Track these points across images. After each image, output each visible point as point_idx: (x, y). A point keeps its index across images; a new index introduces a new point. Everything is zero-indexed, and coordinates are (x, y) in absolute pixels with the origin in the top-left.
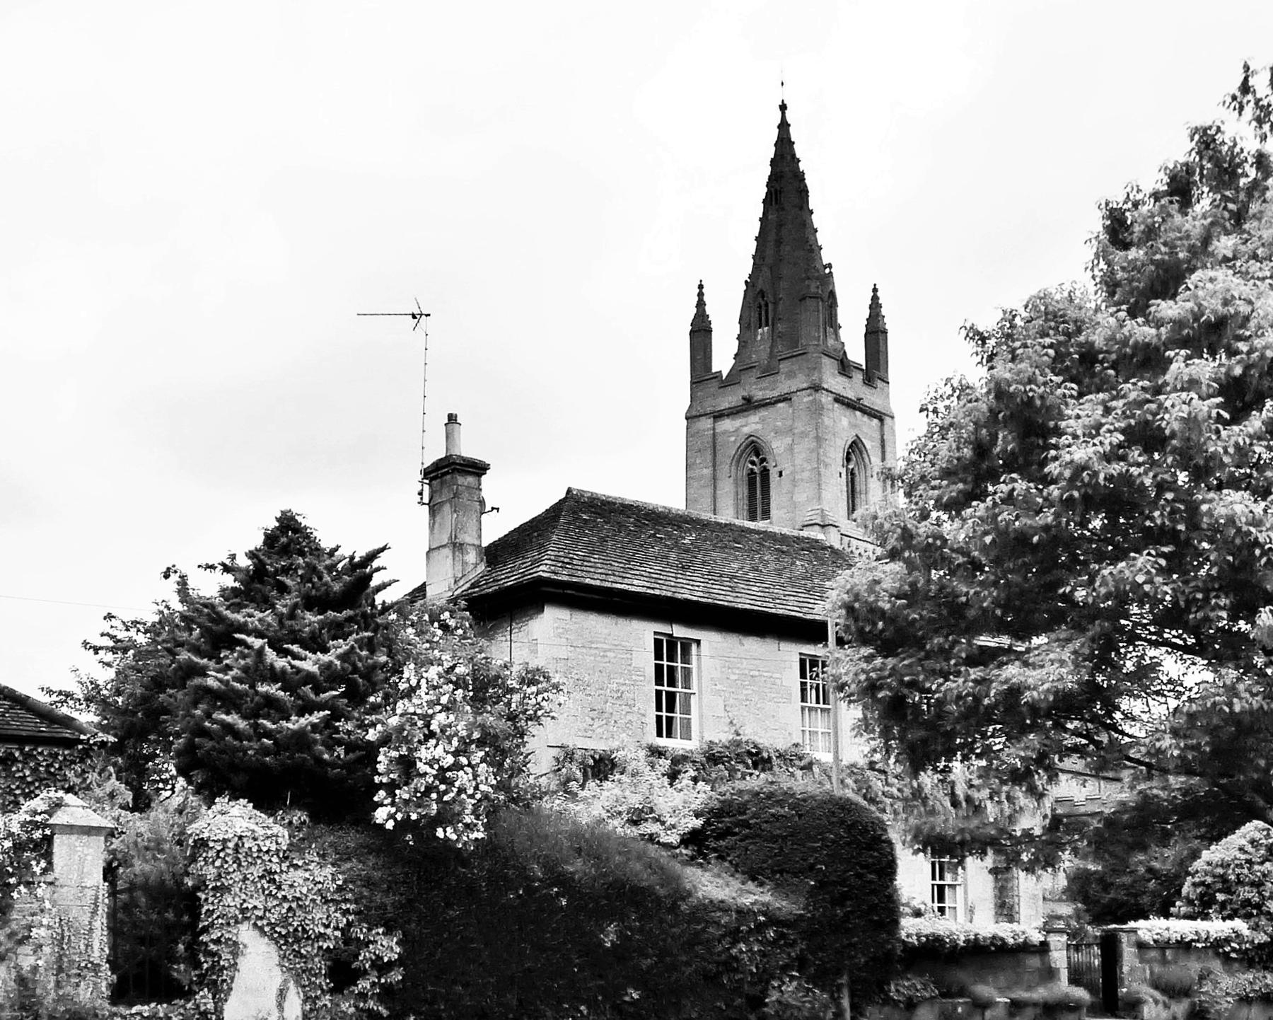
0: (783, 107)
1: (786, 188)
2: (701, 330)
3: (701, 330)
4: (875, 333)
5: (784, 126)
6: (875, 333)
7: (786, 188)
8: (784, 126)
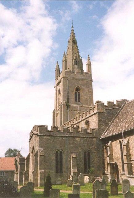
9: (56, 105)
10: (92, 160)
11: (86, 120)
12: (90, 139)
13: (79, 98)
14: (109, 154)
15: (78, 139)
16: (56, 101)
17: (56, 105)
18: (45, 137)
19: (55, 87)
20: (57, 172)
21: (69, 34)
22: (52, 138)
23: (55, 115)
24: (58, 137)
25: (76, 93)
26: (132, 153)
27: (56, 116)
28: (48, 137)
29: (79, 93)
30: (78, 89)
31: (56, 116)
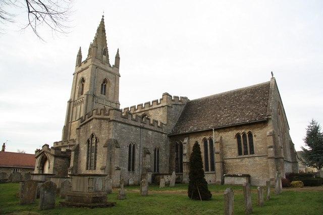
0: (103, 16)
1: (101, 30)
2: (80, 56)
3: (80, 56)
4: (117, 58)
5: (103, 19)
6: (117, 58)
7: (101, 30)
8: (103, 19)
9: (75, 94)
10: (160, 158)
11: (143, 113)
12: (160, 134)
13: (105, 91)
14: (72, 165)
15: (150, 133)
16: (75, 90)
17: (75, 94)
18: (120, 124)
19: (74, 74)
20: (129, 170)
21: (97, 25)
22: (126, 126)
23: (72, 106)
24: (133, 127)
25: (102, 85)
26: (233, 145)
27: (73, 107)
28: (123, 125)
29: (105, 85)
30: (105, 81)
31: (73, 107)
